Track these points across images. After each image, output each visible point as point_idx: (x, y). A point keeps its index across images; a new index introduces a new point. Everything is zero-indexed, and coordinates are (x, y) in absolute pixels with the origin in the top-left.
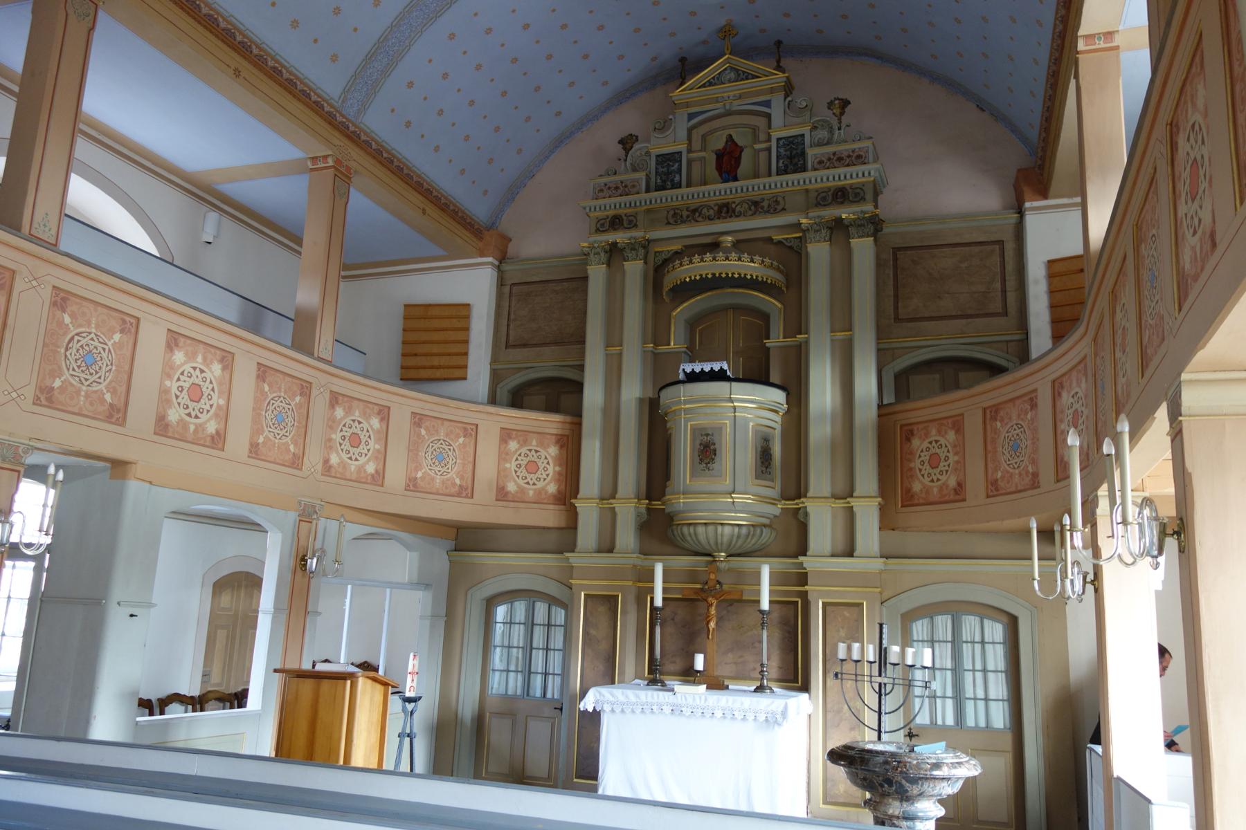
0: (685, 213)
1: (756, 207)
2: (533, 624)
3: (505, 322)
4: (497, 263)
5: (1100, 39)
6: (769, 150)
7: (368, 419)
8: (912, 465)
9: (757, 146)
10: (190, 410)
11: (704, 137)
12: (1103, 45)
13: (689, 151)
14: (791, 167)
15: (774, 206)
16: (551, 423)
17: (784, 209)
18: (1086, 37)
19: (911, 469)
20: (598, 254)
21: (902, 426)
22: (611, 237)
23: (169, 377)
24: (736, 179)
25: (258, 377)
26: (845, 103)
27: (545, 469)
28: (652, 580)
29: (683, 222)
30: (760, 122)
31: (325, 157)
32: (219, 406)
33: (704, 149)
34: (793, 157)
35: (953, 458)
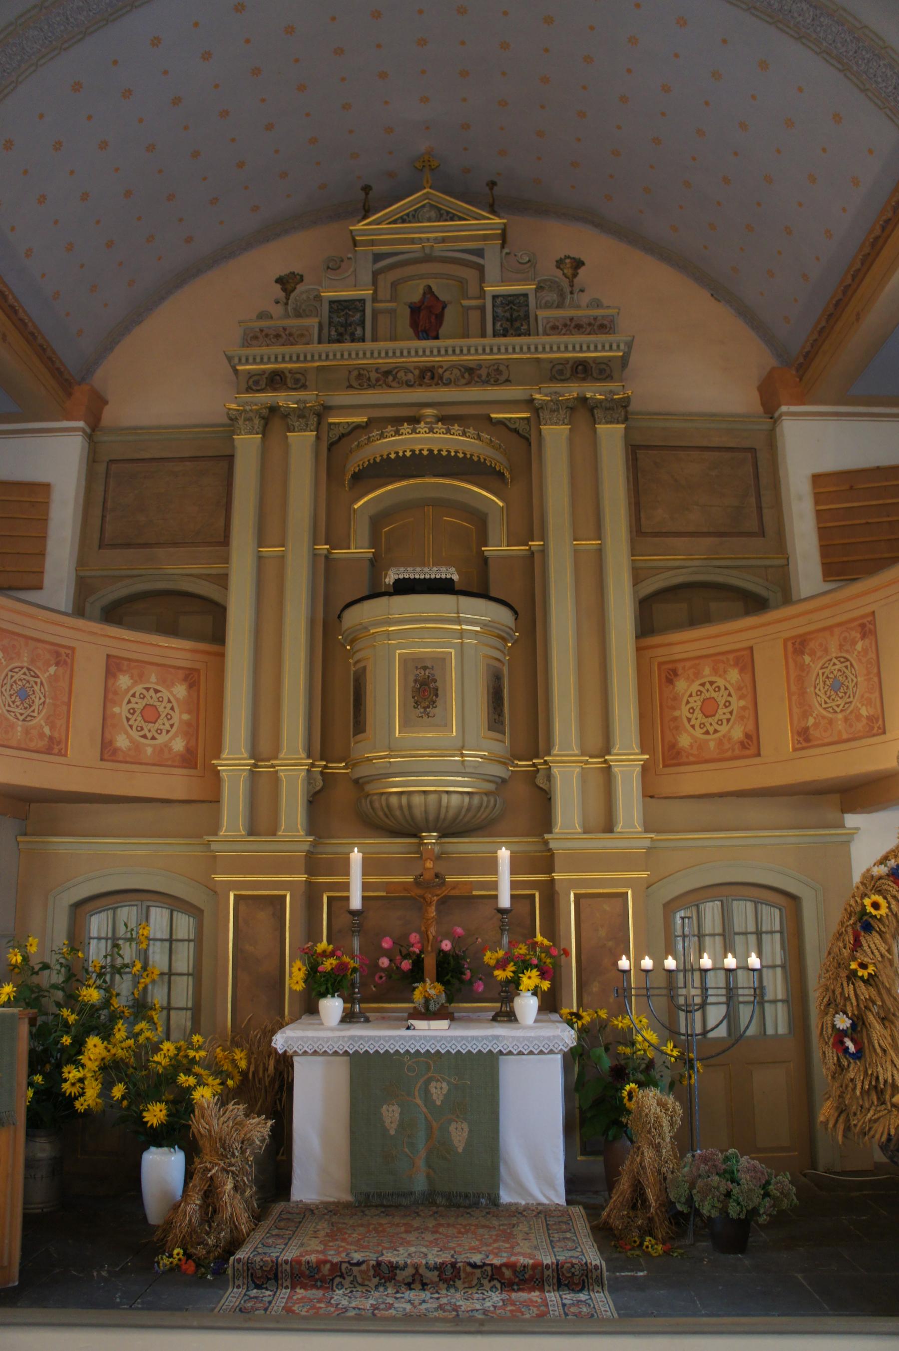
0: (374, 375)
1: (471, 374)
2: (723, 935)
3: (98, 512)
4: (88, 430)
6: (482, 309)
8: (677, 713)
9: (465, 303)
11: (394, 285)
13: (375, 299)
14: (511, 332)
15: (496, 375)
16: (176, 650)
17: (508, 381)
19: (675, 719)
20: (250, 419)
21: (660, 664)
22: (266, 398)
26: (578, 264)
27: (169, 717)
28: (347, 873)
29: (371, 386)
30: (470, 274)
33: (394, 298)
34: (513, 317)
35: (737, 704)
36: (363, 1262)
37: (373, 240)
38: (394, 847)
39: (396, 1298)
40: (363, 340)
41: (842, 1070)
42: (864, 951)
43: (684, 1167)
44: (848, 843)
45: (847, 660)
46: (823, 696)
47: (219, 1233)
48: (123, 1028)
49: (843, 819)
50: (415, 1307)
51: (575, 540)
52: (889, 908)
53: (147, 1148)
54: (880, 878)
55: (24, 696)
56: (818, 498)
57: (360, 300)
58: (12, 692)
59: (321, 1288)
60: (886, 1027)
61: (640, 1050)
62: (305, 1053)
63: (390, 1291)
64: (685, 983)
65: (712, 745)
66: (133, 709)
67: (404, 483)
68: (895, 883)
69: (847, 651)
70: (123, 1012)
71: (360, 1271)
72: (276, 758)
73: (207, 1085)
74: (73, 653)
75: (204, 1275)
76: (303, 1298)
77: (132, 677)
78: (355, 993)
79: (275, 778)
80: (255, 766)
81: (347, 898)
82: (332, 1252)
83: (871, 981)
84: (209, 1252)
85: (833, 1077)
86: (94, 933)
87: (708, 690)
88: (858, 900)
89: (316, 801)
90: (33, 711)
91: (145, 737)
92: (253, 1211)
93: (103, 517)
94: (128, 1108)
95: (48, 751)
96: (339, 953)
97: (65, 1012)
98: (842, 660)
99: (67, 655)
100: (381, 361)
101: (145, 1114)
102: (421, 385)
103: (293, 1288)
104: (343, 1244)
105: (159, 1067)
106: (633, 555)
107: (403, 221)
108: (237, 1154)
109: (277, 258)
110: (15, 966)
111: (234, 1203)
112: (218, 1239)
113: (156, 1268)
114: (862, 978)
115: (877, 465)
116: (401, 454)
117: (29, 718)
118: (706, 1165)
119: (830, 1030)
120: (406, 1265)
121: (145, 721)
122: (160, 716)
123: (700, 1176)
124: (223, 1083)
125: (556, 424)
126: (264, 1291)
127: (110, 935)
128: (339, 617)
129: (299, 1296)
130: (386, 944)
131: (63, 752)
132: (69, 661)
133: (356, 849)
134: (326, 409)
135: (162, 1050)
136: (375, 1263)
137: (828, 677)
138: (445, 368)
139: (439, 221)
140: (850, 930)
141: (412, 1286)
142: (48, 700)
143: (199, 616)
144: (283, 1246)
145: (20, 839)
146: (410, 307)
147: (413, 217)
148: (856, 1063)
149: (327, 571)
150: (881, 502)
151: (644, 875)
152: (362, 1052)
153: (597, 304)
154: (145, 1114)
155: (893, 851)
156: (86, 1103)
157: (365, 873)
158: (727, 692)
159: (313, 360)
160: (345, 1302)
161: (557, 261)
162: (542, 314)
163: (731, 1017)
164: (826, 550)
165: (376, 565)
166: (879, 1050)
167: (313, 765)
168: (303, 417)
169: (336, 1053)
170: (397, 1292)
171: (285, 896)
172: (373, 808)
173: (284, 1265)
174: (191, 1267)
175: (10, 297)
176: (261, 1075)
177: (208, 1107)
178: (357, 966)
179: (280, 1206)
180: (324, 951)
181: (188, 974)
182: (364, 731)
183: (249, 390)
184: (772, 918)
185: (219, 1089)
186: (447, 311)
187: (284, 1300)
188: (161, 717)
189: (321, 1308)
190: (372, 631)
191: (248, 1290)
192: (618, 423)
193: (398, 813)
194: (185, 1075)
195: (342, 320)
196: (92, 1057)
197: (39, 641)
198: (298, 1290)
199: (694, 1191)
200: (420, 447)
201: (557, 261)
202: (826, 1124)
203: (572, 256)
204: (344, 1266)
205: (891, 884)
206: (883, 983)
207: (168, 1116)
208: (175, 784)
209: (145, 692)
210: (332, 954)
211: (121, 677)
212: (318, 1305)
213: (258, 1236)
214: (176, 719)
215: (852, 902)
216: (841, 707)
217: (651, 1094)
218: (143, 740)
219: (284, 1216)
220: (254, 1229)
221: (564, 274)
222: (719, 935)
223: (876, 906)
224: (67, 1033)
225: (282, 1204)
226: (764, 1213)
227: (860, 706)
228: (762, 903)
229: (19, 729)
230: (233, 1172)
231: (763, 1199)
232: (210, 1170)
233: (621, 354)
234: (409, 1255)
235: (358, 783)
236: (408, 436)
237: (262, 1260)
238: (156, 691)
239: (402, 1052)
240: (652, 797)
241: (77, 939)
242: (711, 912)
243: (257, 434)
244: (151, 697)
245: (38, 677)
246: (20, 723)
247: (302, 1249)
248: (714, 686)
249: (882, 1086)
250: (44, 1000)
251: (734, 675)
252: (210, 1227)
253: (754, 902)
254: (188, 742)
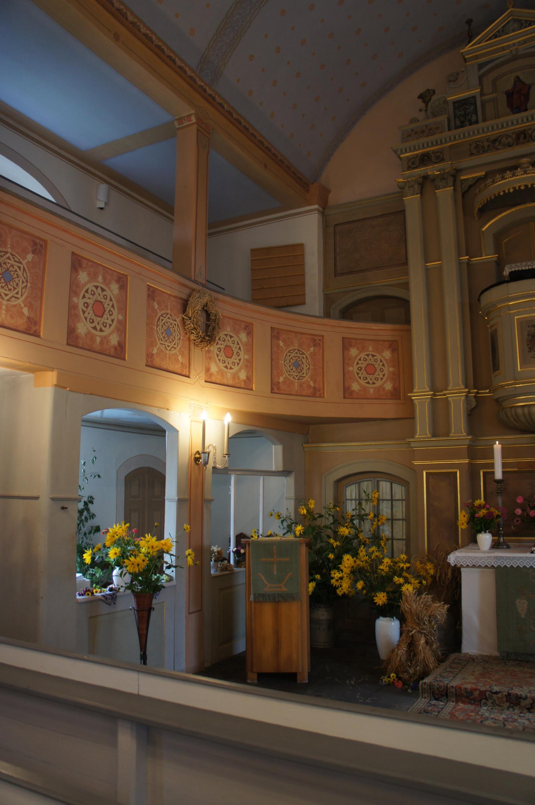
0: (486, 144)
4: (321, 209)
7: (237, 333)
10: (95, 324)
12: (188, 123)
13: (482, 94)
16: (383, 330)
20: (412, 186)
22: (421, 171)
23: (77, 294)
24: (526, 110)
25: (149, 296)
27: (382, 370)
28: (493, 458)
29: (485, 151)
31: (189, 116)
32: (119, 321)
36: (499, 692)
37: (476, 55)
38: (522, 440)
39: (520, 716)
40: (477, 122)
47: (416, 667)
48: (364, 550)
50: (531, 723)
53: (378, 617)
55: (297, 365)
57: (472, 97)
58: (290, 364)
59: (474, 704)
62: (468, 566)
63: (516, 711)
66: (361, 367)
67: (513, 210)
70: (366, 541)
71: (498, 698)
72: (446, 390)
73: (411, 583)
74: (323, 339)
75: (406, 690)
76: (462, 709)
77: (358, 349)
78: (500, 531)
79: (446, 402)
80: (434, 395)
81: (493, 473)
82: (480, 685)
84: (410, 677)
86: (348, 497)
89: (473, 414)
90: (303, 374)
91: (368, 383)
92: (438, 657)
93: (335, 258)
94: (366, 595)
95: (314, 395)
96: (487, 506)
97: (332, 541)
99: (320, 340)
100: (489, 134)
101: (375, 598)
102: (517, 144)
103: (457, 702)
104: (489, 680)
105: (382, 572)
107: (495, 36)
108: (426, 623)
109: (418, 83)
110: (304, 515)
111: (426, 652)
112: (415, 670)
113: (381, 683)
116: (507, 191)
117: (301, 378)
120: (526, 698)
121: (368, 374)
122: (376, 370)
124: (420, 583)
126: (439, 702)
127: (357, 498)
128: (479, 300)
129: (460, 707)
130: (520, 500)
131: (322, 395)
132: (321, 343)
133: (497, 442)
134: (458, 171)
135: (383, 562)
136: (506, 693)
138: (533, 129)
139: (520, 30)
141: (531, 710)
142: (311, 367)
143: (393, 308)
144: (452, 678)
145: (304, 445)
146: (506, 94)
147: (503, 31)
149: (468, 272)
152: (502, 566)
154: (375, 598)
156: (343, 591)
157: (503, 457)
159: (446, 142)
160: (487, 714)
165: (499, 264)
167: (469, 392)
168: (444, 179)
169: (486, 567)
170: (521, 713)
171: (456, 472)
172: (507, 417)
173: (451, 689)
174: (400, 684)
175: (265, 142)
176: (443, 579)
177: (410, 596)
178: (499, 514)
179: (453, 656)
180: (480, 505)
181: (403, 520)
182: (498, 369)
183: (409, 168)
185: (418, 586)
186: (532, 91)
187: (451, 709)
188: (377, 371)
189: (472, 716)
190: (498, 306)
191: (430, 700)
193: (523, 419)
194: (398, 577)
195: (462, 113)
196: (346, 566)
197: (303, 334)
198: (460, 704)
200: (519, 185)
204: (487, 693)
207: (387, 600)
208: (388, 409)
209: (366, 357)
210: (484, 507)
211: (352, 350)
212: (471, 714)
213: (438, 671)
214: (386, 371)
218: (368, 385)
219: (456, 661)
220: (437, 667)
224: (332, 552)
225: (456, 654)
229: (296, 384)
230: (425, 634)
232: (411, 632)
234: (530, 691)
235: (498, 401)
236: (522, 176)
237: (438, 684)
238: (373, 356)
239: (528, 567)
241: (339, 500)
243: (417, 194)
244: (370, 360)
245: (304, 354)
246: (296, 381)
247: (463, 681)
250: (322, 534)
252: (411, 663)
254: (394, 385)
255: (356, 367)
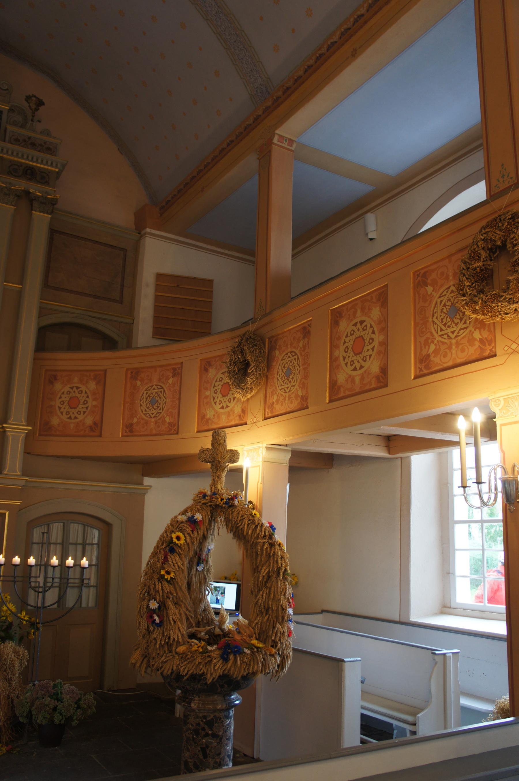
2: (62, 544)
5: (286, 141)
8: (53, 403)
12: (286, 146)
18: (281, 136)
26: (40, 103)
27: (63, 403)
41: (149, 633)
42: (169, 564)
43: (27, 692)
44: (144, 494)
45: (162, 388)
46: (144, 406)
49: (143, 480)
51: (5, 282)
52: (185, 540)
54: (182, 522)
56: (158, 287)
60: (177, 609)
61: (3, 616)
64: (40, 574)
65: (72, 426)
68: (190, 526)
69: (163, 383)
83: (171, 581)
85: (143, 637)
87: (74, 392)
88: (168, 534)
98: (159, 387)
106: (41, 299)
114: (166, 580)
115: (195, 276)
118: (43, 690)
119: (145, 610)
123: (37, 698)
125: (6, 203)
137: (149, 396)
140: (162, 551)
148: (158, 629)
150: (193, 298)
151: (18, 503)
153: (49, 134)
155: (190, 507)
158: (86, 395)
161: (26, 96)
162: (10, 128)
163: (62, 597)
164: (156, 318)
166: (172, 622)
184: (95, 535)
188: (67, 402)
192: (47, 213)
199: (33, 708)
201: (26, 96)
202: (134, 665)
203: (37, 96)
205: (188, 526)
206: (178, 583)
215: (165, 535)
216: (154, 415)
217: (10, 646)
221: (29, 106)
222: (59, 544)
223: (178, 538)
226: (76, 719)
227: (165, 416)
228: (88, 526)
231: (76, 710)
233: (57, 170)
240: (28, 453)
242: (56, 529)
248: (79, 390)
249: (172, 642)
251: (92, 385)
253: (84, 525)
255: (89, 404)
